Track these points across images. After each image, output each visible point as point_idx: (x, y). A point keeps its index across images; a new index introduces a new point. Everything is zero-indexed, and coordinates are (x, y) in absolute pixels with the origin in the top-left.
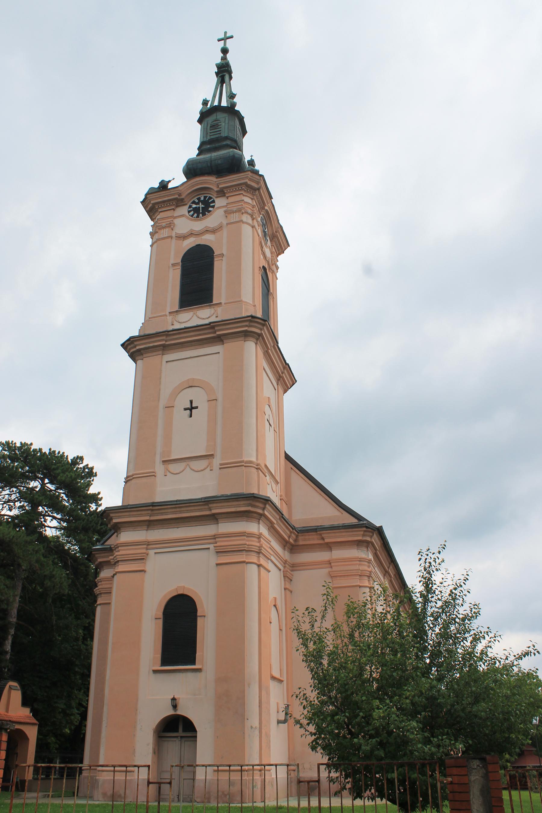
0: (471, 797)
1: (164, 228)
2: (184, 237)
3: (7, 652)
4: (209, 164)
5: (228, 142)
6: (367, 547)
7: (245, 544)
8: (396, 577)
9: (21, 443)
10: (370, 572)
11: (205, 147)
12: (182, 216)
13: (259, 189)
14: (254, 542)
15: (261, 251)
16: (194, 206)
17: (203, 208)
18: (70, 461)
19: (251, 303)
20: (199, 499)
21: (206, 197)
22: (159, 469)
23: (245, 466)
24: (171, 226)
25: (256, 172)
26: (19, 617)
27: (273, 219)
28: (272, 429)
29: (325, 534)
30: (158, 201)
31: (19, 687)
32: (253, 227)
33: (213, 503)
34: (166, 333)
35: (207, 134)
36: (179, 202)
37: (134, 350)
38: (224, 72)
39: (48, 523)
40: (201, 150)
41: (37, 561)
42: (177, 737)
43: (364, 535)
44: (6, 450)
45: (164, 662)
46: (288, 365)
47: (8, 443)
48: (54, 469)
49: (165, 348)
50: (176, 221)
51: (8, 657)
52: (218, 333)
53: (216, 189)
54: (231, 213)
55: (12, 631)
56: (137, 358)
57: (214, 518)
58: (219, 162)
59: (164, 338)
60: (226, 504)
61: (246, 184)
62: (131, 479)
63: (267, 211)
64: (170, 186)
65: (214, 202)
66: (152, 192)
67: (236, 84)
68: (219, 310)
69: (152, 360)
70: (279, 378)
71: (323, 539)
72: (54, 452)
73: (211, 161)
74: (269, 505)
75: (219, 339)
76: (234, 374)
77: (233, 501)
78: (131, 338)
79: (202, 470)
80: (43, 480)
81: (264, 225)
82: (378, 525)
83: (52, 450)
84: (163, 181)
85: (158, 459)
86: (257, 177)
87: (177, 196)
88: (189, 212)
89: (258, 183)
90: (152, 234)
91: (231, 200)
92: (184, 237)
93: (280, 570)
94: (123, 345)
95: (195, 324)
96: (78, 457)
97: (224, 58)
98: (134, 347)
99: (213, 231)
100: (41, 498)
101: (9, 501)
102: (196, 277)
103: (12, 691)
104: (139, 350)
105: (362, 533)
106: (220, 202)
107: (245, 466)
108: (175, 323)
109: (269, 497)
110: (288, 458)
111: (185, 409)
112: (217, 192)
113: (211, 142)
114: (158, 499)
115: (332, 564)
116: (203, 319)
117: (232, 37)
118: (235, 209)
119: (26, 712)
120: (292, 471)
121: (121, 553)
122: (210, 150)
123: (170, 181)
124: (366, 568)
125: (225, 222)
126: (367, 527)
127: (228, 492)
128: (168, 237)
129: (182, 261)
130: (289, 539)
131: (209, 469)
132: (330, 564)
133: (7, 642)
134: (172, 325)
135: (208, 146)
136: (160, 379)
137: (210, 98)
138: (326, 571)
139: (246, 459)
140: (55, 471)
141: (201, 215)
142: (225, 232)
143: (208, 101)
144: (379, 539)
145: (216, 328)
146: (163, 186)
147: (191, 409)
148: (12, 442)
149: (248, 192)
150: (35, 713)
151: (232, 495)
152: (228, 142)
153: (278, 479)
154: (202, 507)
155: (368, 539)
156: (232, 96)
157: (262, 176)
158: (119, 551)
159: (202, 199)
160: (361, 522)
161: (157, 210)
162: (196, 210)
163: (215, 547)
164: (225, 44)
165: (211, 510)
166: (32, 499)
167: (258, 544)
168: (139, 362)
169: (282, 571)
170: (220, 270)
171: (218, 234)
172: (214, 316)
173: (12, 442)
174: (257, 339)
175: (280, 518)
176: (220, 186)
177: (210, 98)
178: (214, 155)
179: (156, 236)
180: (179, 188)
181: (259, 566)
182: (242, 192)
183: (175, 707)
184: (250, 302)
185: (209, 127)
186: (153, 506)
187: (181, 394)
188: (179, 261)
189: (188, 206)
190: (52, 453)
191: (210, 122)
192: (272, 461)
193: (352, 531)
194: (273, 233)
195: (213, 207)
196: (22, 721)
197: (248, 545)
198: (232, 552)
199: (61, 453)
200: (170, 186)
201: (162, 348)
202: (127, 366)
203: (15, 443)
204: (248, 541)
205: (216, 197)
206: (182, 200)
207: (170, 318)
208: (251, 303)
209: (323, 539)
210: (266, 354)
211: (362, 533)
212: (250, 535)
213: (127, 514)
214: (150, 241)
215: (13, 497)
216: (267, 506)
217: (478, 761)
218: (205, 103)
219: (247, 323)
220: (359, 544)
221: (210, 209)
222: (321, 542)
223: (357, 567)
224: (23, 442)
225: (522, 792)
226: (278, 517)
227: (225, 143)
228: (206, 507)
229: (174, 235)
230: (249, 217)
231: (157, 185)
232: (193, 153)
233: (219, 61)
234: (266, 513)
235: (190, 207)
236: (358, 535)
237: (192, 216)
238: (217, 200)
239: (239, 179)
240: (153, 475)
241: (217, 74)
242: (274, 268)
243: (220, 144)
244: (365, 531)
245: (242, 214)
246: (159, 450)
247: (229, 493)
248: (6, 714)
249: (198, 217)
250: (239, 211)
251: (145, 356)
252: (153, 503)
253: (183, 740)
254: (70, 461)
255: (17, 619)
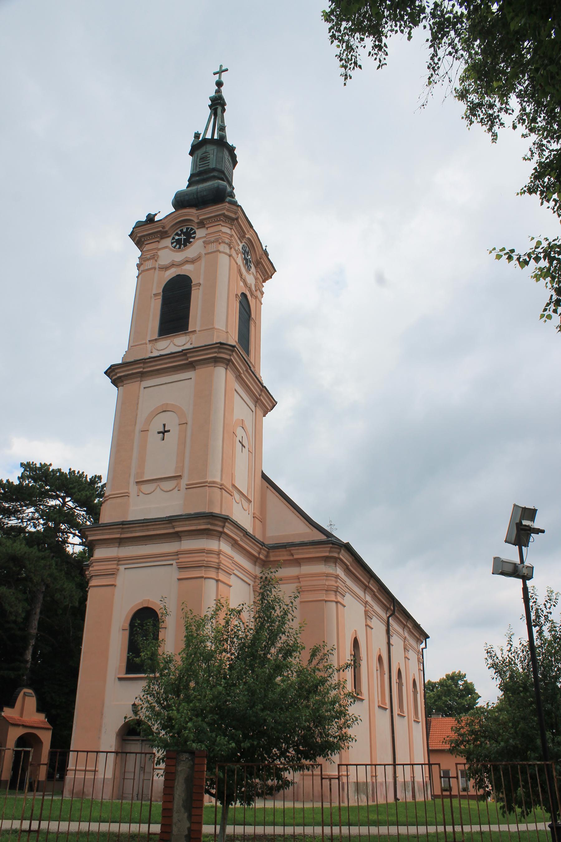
0: (176, 784)
1: (148, 259)
2: (166, 268)
3: (27, 662)
4: (195, 196)
5: (215, 174)
6: (335, 563)
7: (204, 561)
8: (380, 591)
9: (41, 464)
10: (337, 587)
11: (194, 179)
12: (166, 247)
13: (237, 219)
14: (214, 559)
15: (239, 278)
16: (177, 237)
17: (184, 239)
18: (89, 480)
19: (224, 330)
20: (164, 518)
21: (188, 228)
22: (133, 489)
23: (209, 487)
24: (154, 257)
25: (235, 204)
26: (39, 629)
27: (257, 247)
28: (246, 450)
29: (294, 550)
30: (146, 233)
31: (33, 694)
32: (230, 256)
33: (176, 522)
34: (144, 361)
35: (196, 166)
36: (163, 235)
37: (115, 377)
38: (217, 104)
39: (70, 540)
40: (191, 182)
41: (51, 575)
42: (138, 740)
43: (330, 552)
44: (27, 471)
45: (128, 671)
46: (265, 387)
47: (28, 464)
48: (71, 488)
49: (143, 375)
50: (160, 253)
51: (29, 665)
52: (190, 360)
53: (196, 221)
54: (209, 244)
55: (33, 642)
56: (119, 385)
57: (177, 536)
58: (205, 193)
59: (142, 365)
60: (187, 522)
61: (224, 215)
62: (107, 500)
63: (249, 239)
64: (157, 219)
65: (195, 233)
66: (139, 225)
67: (229, 116)
68: (194, 337)
69: (132, 386)
70: (257, 401)
71: (292, 555)
72: (74, 471)
73: (197, 193)
74: (229, 523)
75: (192, 366)
76: (204, 398)
77: (186, 521)
78: (112, 366)
79: (170, 491)
80: (63, 498)
81: (245, 253)
82: (345, 541)
83: (72, 470)
84: (149, 215)
85: (132, 480)
86: (235, 208)
87: (161, 229)
88: (172, 243)
89: (236, 213)
90: (139, 266)
91: (211, 230)
92: (166, 268)
93: (249, 585)
94: (106, 373)
95: (169, 352)
96: (96, 476)
97: (218, 91)
98: (117, 374)
99: (192, 261)
100: (55, 516)
101: (33, 518)
102: (174, 305)
103: (26, 697)
104: (120, 378)
105: (329, 549)
106: (200, 233)
107: (209, 487)
108: (154, 350)
109: (228, 516)
110: (264, 477)
111: (159, 433)
112: (197, 223)
113: (199, 174)
114: (130, 518)
115: (301, 579)
116: (179, 346)
117: (227, 70)
118: (212, 239)
119: (41, 718)
120: (268, 490)
121: (95, 568)
122: (198, 182)
123: (156, 214)
124: (333, 583)
125: (203, 252)
126: (333, 544)
127: (192, 510)
128: (151, 269)
129: (163, 291)
130: (259, 555)
131: (177, 489)
132: (299, 579)
133: (27, 652)
134: (151, 352)
135: (197, 178)
136: (138, 404)
137: (202, 132)
138: (295, 585)
139: (209, 480)
140: (72, 490)
141: (182, 246)
142: (203, 262)
143: (200, 134)
144: (349, 555)
145: (188, 355)
146: (150, 219)
147: (164, 432)
148: (33, 462)
149: (226, 222)
150: (51, 719)
151: (195, 514)
152: (215, 174)
153: (251, 498)
154: (165, 526)
155: (336, 555)
156: (222, 129)
157: (240, 207)
158: (93, 567)
159: (185, 230)
160: (330, 539)
161: (143, 243)
162: (178, 242)
163: (177, 563)
164: (220, 77)
165: (174, 528)
166: (52, 515)
167: (217, 561)
168: (120, 388)
169: (251, 586)
170: (197, 298)
171: (197, 264)
172: (189, 343)
173: (33, 462)
174: (227, 365)
175: (244, 535)
176: (200, 218)
177: (202, 132)
178: (201, 186)
179: (142, 268)
180: (163, 221)
181: (337, 602)
182: (221, 223)
183: (136, 712)
184: (226, 328)
185: (198, 160)
186: (123, 524)
187: (154, 420)
188: (160, 291)
189: (171, 238)
190: (72, 472)
191: (200, 154)
192: (243, 479)
193: (320, 548)
194: (257, 260)
195: (194, 238)
196: (36, 725)
197: (207, 561)
198: (193, 568)
199: (81, 473)
200: (157, 219)
201: (140, 375)
202: (110, 392)
203: (36, 464)
204: (207, 557)
205: (197, 229)
206: (166, 232)
207: (149, 346)
208: (224, 330)
209: (292, 555)
210: (239, 377)
211: (329, 549)
212: (210, 552)
213: (100, 532)
214: (136, 272)
215: (37, 515)
216: (227, 524)
217: (188, 754)
218: (197, 136)
219: (216, 350)
220: (326, 560)
221: (191, 240)
222: (291, 558)
223: (324, 582)
224: (43, 463)
225: (470, 800)
226: (242, 535)
227: (212, 174)
228: (170, 525)
229: (157, 266)
230: (226, 246)
231: (144, 219)
232: (182, 184)
233: (213, 94)
234: (226, 530)
235: (173, 238)
236: (324, 552)
237: (175, 247)
238: (198, 232)
239: (217, 211)
240: (126, 495)
241: (210, 107)
242: (259, 294)
243: (208, 176)
244: (331, 547)
245: (220, 244)
246: (133, 471)
247: (192, 512)
248: (20, 718)
249: (180, 248)
250: (217, 241)
251: (125, 382)
252: (123, 522)
253: (144, 743)
254: (89, 480)
255: (38, 630)
